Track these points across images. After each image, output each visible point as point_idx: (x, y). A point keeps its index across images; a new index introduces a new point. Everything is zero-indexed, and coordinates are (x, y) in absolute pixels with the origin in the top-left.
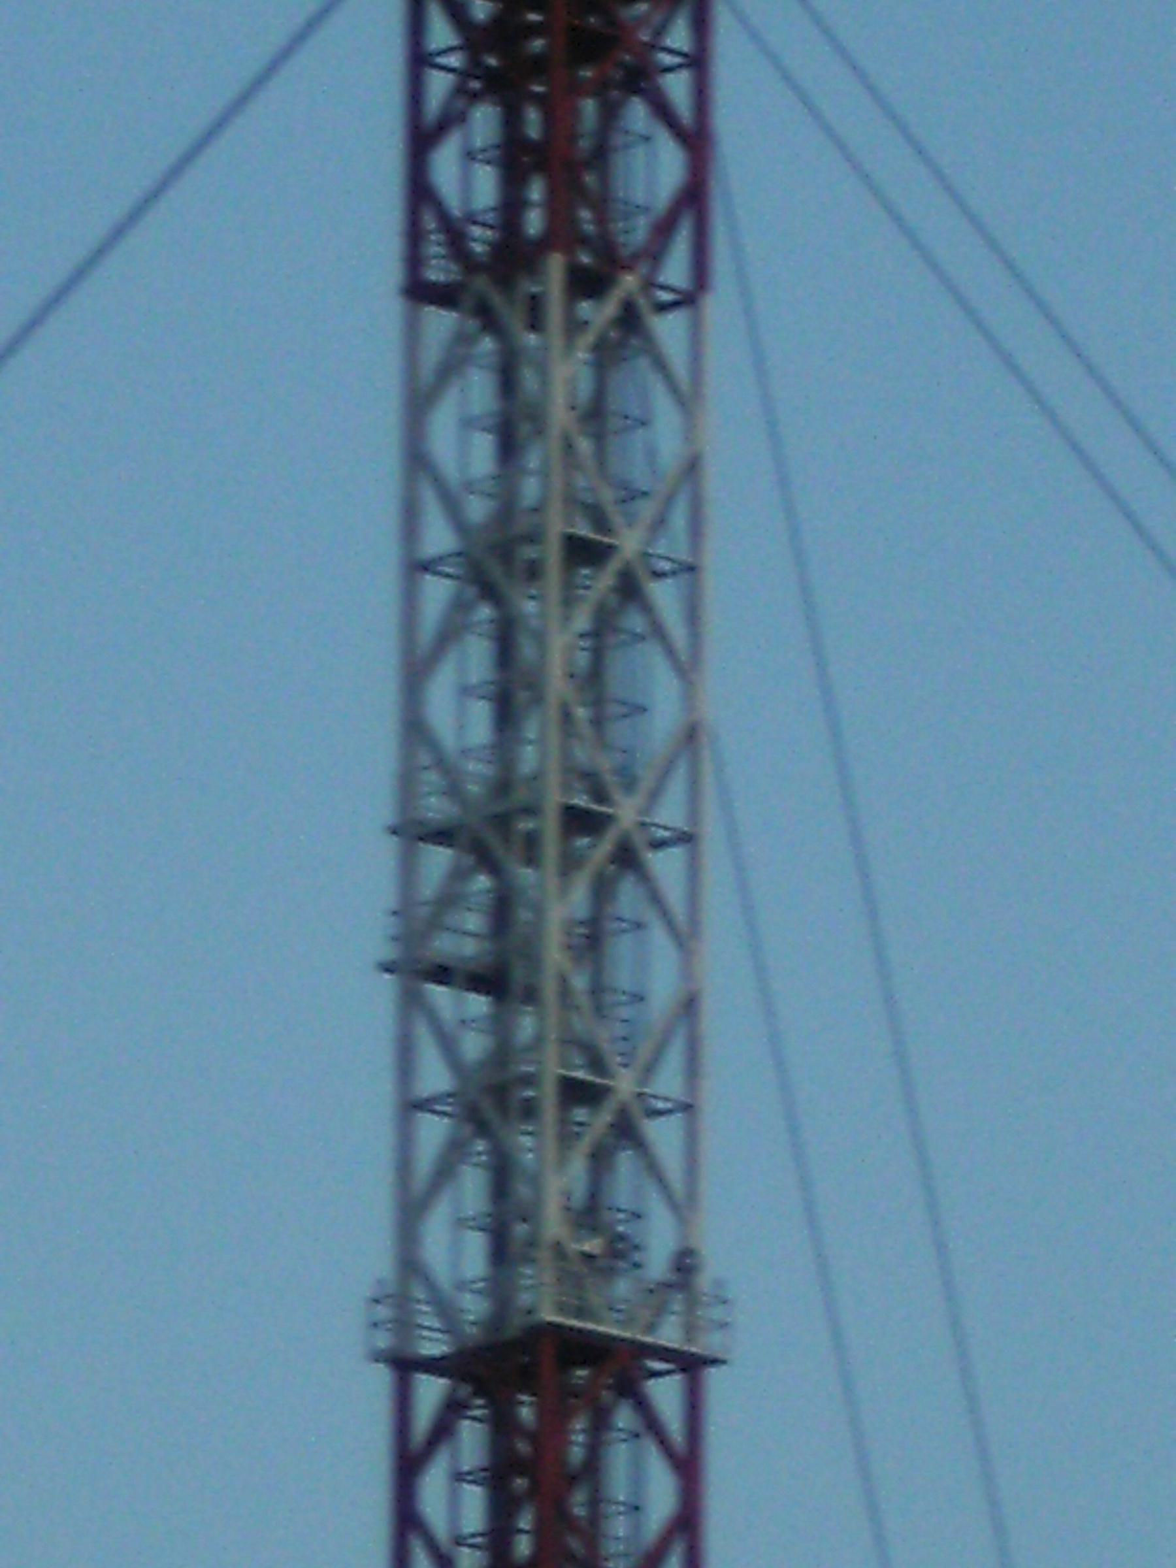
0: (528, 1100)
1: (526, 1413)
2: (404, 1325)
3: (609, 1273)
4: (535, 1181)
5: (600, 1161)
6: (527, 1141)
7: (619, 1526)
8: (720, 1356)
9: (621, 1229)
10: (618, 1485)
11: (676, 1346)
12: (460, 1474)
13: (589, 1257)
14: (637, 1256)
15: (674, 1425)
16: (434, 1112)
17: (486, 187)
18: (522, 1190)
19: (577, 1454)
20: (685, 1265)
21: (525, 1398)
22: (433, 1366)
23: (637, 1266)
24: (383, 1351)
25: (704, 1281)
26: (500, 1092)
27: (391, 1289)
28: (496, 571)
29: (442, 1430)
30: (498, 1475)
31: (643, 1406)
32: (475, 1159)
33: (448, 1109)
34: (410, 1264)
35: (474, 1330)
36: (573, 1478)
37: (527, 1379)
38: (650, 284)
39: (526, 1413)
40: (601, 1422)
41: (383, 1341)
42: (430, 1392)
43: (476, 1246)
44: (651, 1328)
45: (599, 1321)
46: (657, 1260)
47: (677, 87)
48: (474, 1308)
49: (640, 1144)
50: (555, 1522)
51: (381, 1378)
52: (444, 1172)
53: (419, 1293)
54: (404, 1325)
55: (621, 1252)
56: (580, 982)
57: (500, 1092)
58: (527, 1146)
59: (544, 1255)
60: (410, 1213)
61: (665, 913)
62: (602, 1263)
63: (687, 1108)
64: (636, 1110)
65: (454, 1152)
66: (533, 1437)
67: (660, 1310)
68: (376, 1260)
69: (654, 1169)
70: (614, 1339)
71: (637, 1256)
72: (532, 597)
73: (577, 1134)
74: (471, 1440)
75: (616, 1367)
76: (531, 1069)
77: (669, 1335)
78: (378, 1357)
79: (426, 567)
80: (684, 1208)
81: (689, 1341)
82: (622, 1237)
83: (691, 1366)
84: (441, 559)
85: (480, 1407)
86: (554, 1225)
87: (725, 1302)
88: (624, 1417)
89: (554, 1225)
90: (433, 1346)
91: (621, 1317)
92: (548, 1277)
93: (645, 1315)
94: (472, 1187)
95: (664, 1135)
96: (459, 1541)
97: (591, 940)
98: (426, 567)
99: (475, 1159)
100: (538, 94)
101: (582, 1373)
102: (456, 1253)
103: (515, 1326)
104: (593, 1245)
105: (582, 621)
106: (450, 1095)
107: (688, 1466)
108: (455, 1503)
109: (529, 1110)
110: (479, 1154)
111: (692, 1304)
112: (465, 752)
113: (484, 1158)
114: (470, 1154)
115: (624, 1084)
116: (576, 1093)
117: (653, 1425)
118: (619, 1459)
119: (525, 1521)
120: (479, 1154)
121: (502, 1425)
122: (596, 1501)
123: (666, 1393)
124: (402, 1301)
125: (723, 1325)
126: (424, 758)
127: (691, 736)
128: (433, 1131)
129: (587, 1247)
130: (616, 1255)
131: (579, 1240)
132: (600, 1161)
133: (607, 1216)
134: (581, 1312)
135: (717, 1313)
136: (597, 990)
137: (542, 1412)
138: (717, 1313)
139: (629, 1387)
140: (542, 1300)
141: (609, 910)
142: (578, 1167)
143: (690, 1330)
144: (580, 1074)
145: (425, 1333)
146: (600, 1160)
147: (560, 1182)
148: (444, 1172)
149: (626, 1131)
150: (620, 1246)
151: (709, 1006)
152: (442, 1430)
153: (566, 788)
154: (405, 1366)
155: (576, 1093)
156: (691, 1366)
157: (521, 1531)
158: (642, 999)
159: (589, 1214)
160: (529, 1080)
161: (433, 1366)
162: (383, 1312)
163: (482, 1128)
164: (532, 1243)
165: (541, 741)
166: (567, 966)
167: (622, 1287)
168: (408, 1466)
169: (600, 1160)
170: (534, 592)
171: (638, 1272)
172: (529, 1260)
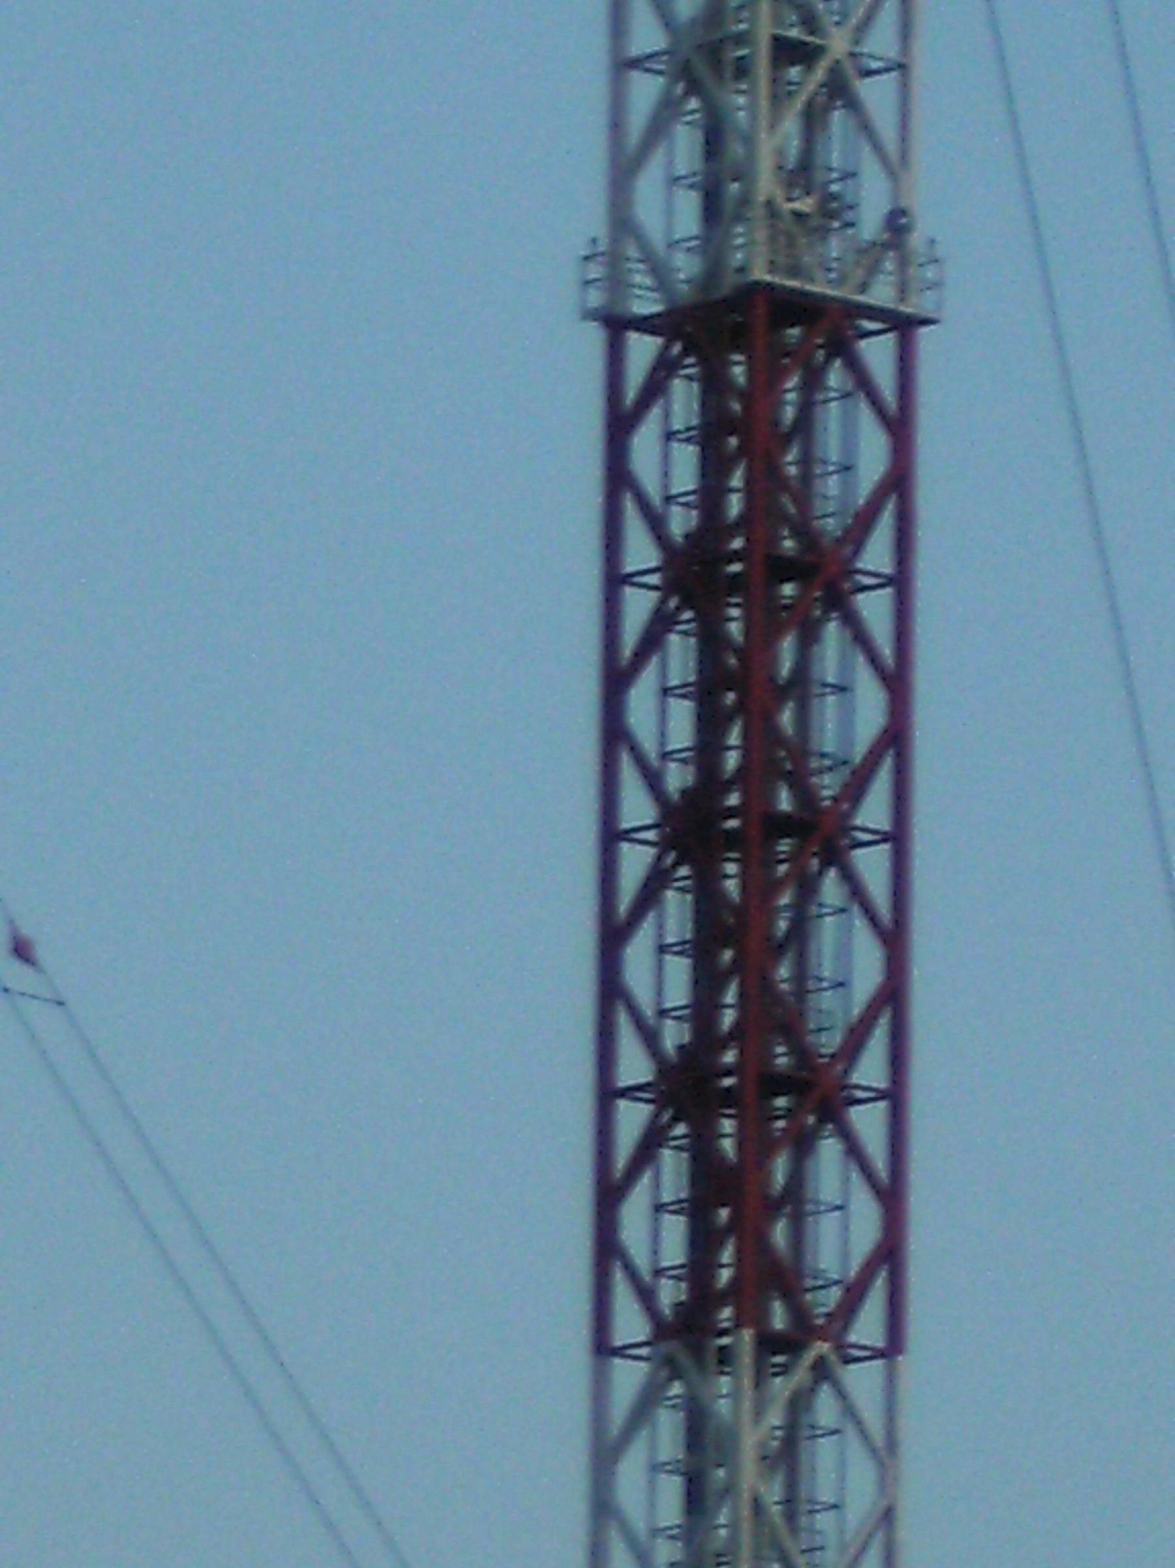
0: (722, 1349)
1: (739, 372)
2: (616, 282)
3: (823, 233)
4: (749, 140)
5: (813, 121)
6: (741, 100)
7: (832, 486)
8: (931, 315)
9: (834, 188)
10: (830, 444)
11: (892, 306)
12: (663, 1205)
13: (798, 216)
14: (849, 216)
15: (872, 1417)
16: (648, 70)
17: (675, 1238)
18: (735, 150)
19: (789, 414)
20: (897, 224)
21: (737, 357)
22: (645, 325)
23: (851, 225)
24: (596, 309)
25: (916, 240)
26: (713, 52)
27: (602, 247)
28: (702, 69)
29: (654, 389)
30: (710, 435)
31: (850, 878)
32: (689, 118)
33: (662, 67)
34: (622, 221)
35: (685, 287)
36: (781, 946)
37: (739, 338)
38: (841, 1347)
39: (739, 372)
40: (813, 381)
41: (595, 298)
42: (642, 350)
43: (689, 206)
44: (863, 288)
45: (812, 280)
46: (870, 224)
47: (875, 608)
48: (686, 267)
49: (853, 104)
50: (766, 481)
51: (594, 337)
52: (657, 129)
53: (632, 251)
54: (616, 282)
55: (835, 210)
56: (773, 1493)
57: (713, 52)
58: (738, 104)
59: (757, 212)
60: (623, 173)
61: (878, 148)
62: (816, 221)
63: (902, 67)
64: (849, 69)
65: (647, 1403)
66: (739, 652)
67: (874, 269)
68: (590, 220)
69: (866, 127)
70: (824, 297)
71: (849, 216)
72: (743, 92)
73: (790, 93)
74: (683, 400)
75: (832, 327)
76: (743, 27)
77: (882, 294)
78: (590, 315)
79: (635, 63)
80: (896, 168)
81: (902, 300)
82: (834, 197)
83: (904, 326)
84: (650, 56)
85: (688, 621)
86: (766, 184)
87: (936, 261)
88: (836, 377)
89: (766, 184)
90: (646, 305)
91: (833, 275)
92: (761, 235)
93: (859, 275)
94: (684, 146)
95: (877, 95)
96: (658, 1272)
97: (787, 1455)
98: (635, 63)
99: (689, 118)
100: (731, 817)
101: (795, 332)
102: (668, 212)
103: (729, 283)
104: (805, 205)
105: (775, 1417)
106: (664, 53)
107: (899, 427)
108: (650, 1495)
109: (742, 70)
110: (692, 112)
111: (903, 263)
112: (673, 245)
113: (697, 116)
114: (668, 1140)
115: (838, 43)
116: (788, 52)
117: (863, 383)
118: (827, 933)
119: (734, 737)
120: (692, 112)
121: (713, 384)
122: (806, 461)
123: (878, 353)
124: (614, 260)
125: (936, 285)
126: (632, 251)
127: (897, 224)
128: (645, 91)
129: (797, 205)
130: (831, 215)
131: (790, 200)
132: (813, 121)
133: (819, 176)
134: (795, 271)
135: (930, 273)
136: (790, 1501)
137: (751, 372)
138: (930, 273)
139: (841, 347)
140: (753, 258)
141: (805, 1420)
142: (791, 126)
143: (903, 291)
144: (794, 33)
145: (638, 292)
146: (813, 120)
147: (775, 141)
148: (657, 129)
149: (838, 89)
150: (835, 205)
151: (907, 1532)
152: (654, 389)
153: (777, 20)
154: (617, 325)
155: (788, 52)
156: (904, 326)
157: (732, 490)
158: (854, 175)
159: (801, 173)
160: (740, 39)
161: (645, 325)
162: (595, 271)
163: (694, 87)
164: (745, 200)
165: (733, 1526)
166: (779, 194)
167: (835, 247)
168: (620, 425)
169: (813, 120)
170: (744, 87)
171: (850, 231)
172: (738, 218)
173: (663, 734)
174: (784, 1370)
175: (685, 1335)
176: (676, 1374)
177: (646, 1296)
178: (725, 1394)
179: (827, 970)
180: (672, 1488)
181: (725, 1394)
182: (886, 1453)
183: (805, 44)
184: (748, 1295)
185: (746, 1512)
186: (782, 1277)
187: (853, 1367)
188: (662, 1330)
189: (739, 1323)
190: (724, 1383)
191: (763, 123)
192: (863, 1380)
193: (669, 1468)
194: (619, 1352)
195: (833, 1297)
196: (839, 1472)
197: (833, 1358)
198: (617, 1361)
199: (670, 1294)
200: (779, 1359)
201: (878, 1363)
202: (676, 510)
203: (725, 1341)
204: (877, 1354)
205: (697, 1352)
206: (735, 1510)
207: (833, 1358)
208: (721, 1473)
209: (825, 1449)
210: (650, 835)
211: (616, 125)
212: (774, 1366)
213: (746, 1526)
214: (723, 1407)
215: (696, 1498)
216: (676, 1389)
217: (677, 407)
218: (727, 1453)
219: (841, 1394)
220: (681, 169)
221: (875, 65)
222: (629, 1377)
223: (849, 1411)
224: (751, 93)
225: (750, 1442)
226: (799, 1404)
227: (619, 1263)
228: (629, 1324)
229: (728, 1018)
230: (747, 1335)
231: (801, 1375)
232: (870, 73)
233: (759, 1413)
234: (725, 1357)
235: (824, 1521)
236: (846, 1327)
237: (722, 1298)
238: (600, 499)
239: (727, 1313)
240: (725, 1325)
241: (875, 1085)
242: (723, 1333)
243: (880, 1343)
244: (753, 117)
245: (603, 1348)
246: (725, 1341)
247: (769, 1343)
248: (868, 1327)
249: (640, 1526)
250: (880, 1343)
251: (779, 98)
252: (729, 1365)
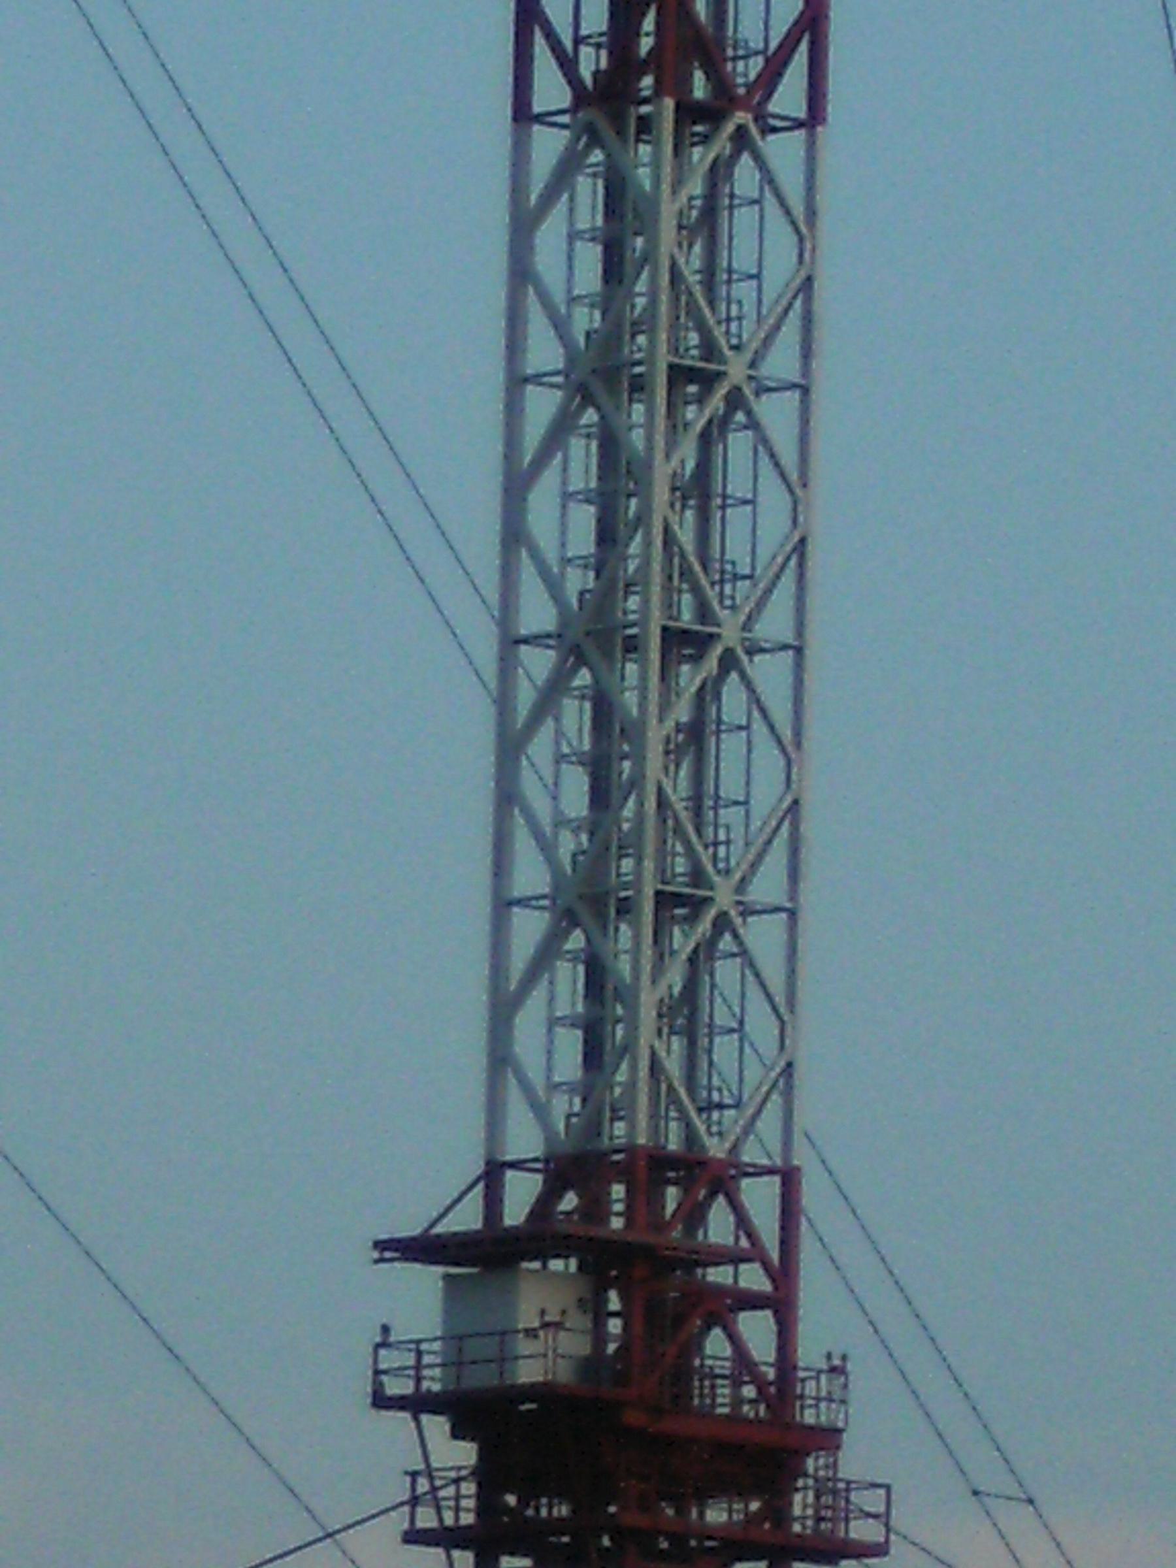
0: (641, 118)
38: (760, 117)
56: (693, 263)
65: (560, 430)
76: (630, 893)
97: (707, 221)
105: (696, 187)
116: (683, 643)
136: (709, 273)
151: (815, 826)
155: (683, 643)
173: (549, 1069)
174: (705, 139)
175: (607, 103)
176: (595, 140)
177: (567, 64)
178: (645, 164)
179: (722, 1018)
180: (590, 257)
181: (645, 164)
182: (805, 226)
183: (693, 896)
184: (669, 67)
185: (651, 804)
186: (704, 46)
187: (771, 138)
188: (581, 98)
189: (659, 90)
190: (644, 150)
191: (666, 188)
192: (784, 151)
193: (580, 497)
194: (539, 119)
195: (756, 66)
196: (757, 242)
197: (754, 130)
198: (536, 128)
199: (589, 62)
200: (699, 128)
201: (800, 134)
202: (586, 52)
203: (645, 109)
204: (798, 124)
205: (618, 122)
206: (634, 1068)
207: (754, 130)
208: (639, 242)
209: (745, 218)
210: (565, 119)
211: (503, 702)
212: (694, 135)
213: (664, 298)
214: (644, 175)
215: (601, 795)
216: (597, 156)
217: (576, 466)
218: (647, 224)
219: (735, 1206)
220: (562, 1009)
221: (773, 384)
222: (548, 144)
223: (768, 178)
224: (656, 144)
225: (656, 735)
226: (718, 173)
227: (509, 1069)
228: (550, 90)
229: (646, 44)
230: (669, 103)
231: (722, 144)
232: (774, 130)
233: (677, 184)
234: (645, 126)
235: (729, 815)
236: (769, 95)
237: (643, 67)
238: (489, 909)
239: (647, 81)
240: (646, 93)
241: (794, 115)
242: (646, 101)
243: (801, 113)
244: (657, 181)
245: (523, 113)
246: (645, 109)
247: (688, 112)
248: (789, 97)
249: (551, 556)
250: (801, 113)
251: (675, 426)
252: (649, 132)
